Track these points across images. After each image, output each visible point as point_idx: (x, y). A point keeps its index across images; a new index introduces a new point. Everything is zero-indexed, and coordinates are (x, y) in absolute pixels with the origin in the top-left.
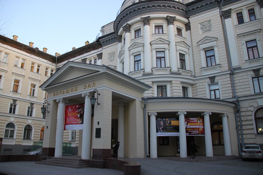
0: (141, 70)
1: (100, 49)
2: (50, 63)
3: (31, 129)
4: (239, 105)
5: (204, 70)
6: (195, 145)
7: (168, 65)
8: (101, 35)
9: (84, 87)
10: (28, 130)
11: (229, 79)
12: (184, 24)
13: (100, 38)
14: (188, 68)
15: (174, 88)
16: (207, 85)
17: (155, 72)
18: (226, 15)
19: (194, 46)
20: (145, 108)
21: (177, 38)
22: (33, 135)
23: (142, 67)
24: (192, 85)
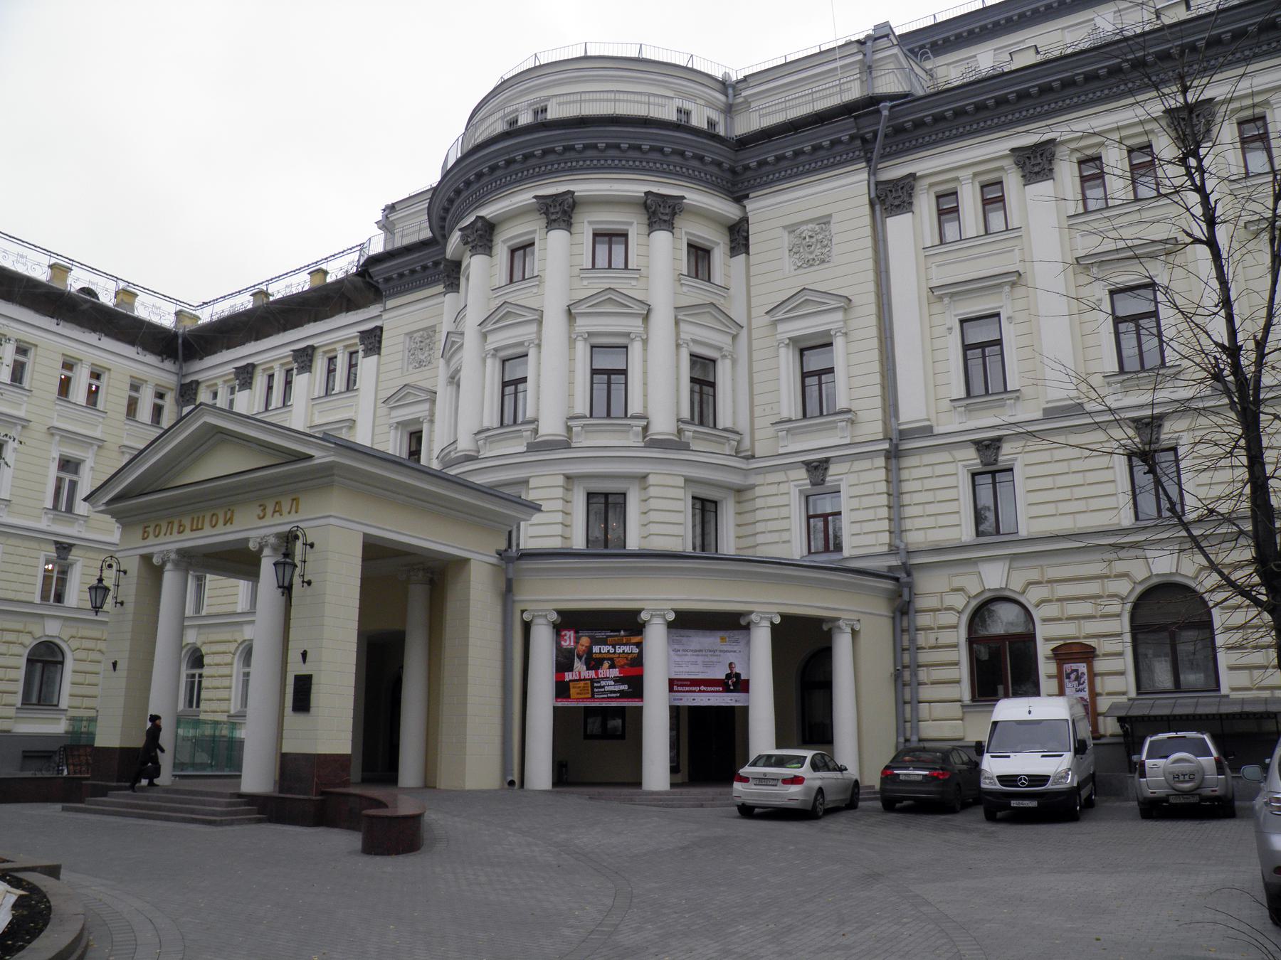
0: (524, 423)
1: (374, 310)
2: (151, 359)
3: (60, 659)
4: (910, 586)
5: (788, 430)
6: (710, 744)
7: (635, 407)
8: (377, 248)
9: (259, 511)
10: (45, 663)
11: (882, 474)
12: (721, 224)
13: (374, 260)
14: (724, 419)
15: (653, 504)
16: (795, 493)
17: (578, 435)
18: (891, 198)
19: (755, 323)
20: (507, 592)
21: (685, 289)
22: (66, 688)
23: (530, 414)
24: (739, 491)
